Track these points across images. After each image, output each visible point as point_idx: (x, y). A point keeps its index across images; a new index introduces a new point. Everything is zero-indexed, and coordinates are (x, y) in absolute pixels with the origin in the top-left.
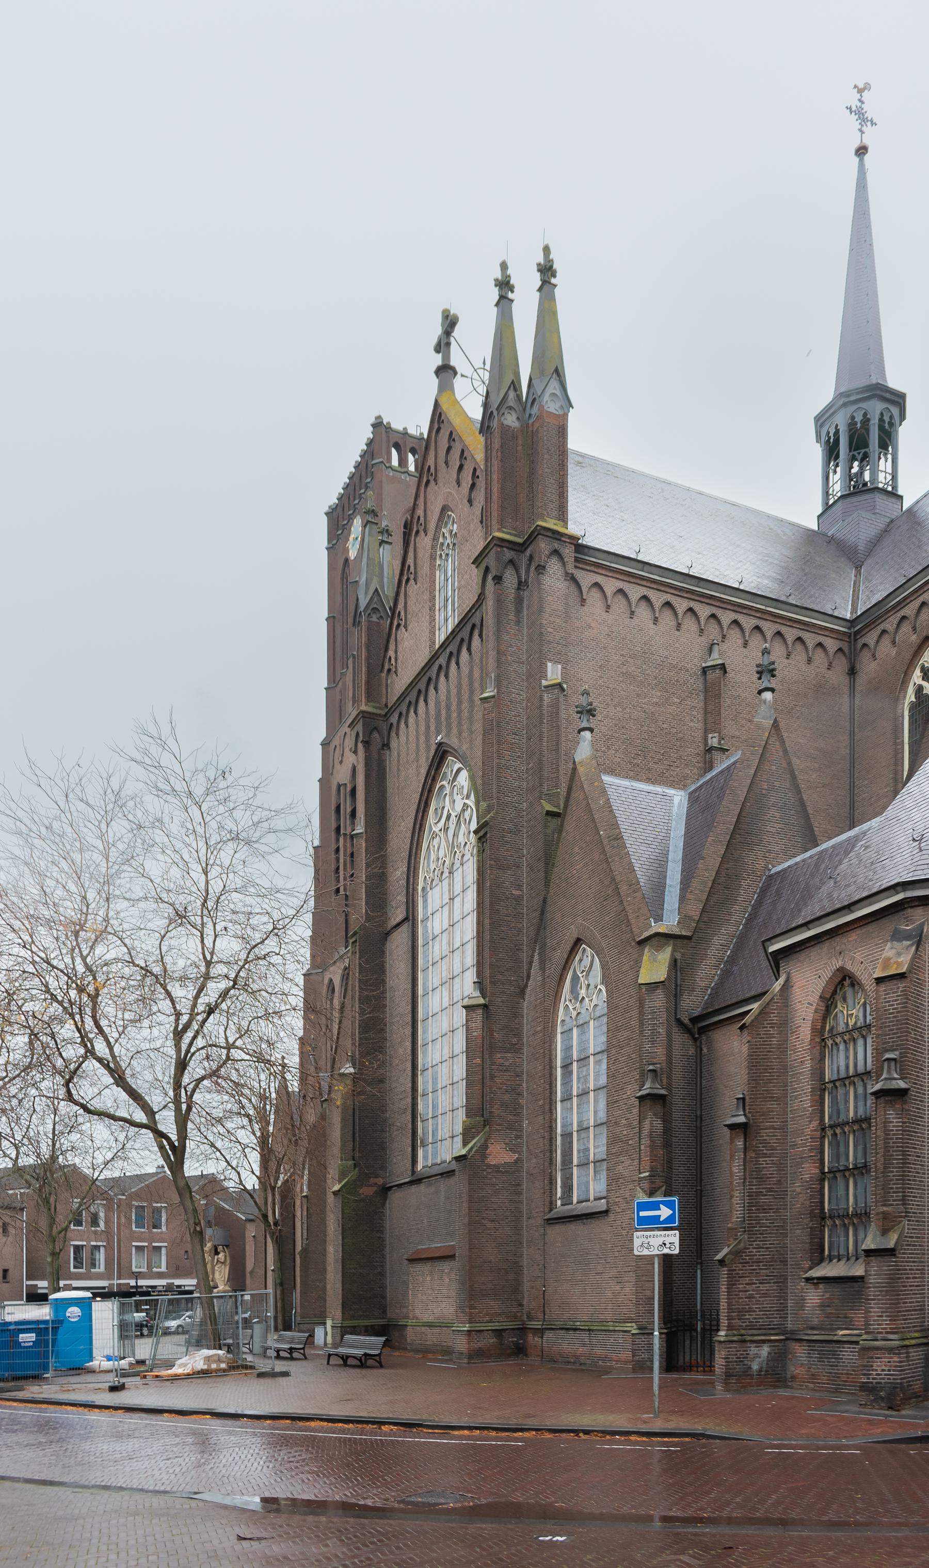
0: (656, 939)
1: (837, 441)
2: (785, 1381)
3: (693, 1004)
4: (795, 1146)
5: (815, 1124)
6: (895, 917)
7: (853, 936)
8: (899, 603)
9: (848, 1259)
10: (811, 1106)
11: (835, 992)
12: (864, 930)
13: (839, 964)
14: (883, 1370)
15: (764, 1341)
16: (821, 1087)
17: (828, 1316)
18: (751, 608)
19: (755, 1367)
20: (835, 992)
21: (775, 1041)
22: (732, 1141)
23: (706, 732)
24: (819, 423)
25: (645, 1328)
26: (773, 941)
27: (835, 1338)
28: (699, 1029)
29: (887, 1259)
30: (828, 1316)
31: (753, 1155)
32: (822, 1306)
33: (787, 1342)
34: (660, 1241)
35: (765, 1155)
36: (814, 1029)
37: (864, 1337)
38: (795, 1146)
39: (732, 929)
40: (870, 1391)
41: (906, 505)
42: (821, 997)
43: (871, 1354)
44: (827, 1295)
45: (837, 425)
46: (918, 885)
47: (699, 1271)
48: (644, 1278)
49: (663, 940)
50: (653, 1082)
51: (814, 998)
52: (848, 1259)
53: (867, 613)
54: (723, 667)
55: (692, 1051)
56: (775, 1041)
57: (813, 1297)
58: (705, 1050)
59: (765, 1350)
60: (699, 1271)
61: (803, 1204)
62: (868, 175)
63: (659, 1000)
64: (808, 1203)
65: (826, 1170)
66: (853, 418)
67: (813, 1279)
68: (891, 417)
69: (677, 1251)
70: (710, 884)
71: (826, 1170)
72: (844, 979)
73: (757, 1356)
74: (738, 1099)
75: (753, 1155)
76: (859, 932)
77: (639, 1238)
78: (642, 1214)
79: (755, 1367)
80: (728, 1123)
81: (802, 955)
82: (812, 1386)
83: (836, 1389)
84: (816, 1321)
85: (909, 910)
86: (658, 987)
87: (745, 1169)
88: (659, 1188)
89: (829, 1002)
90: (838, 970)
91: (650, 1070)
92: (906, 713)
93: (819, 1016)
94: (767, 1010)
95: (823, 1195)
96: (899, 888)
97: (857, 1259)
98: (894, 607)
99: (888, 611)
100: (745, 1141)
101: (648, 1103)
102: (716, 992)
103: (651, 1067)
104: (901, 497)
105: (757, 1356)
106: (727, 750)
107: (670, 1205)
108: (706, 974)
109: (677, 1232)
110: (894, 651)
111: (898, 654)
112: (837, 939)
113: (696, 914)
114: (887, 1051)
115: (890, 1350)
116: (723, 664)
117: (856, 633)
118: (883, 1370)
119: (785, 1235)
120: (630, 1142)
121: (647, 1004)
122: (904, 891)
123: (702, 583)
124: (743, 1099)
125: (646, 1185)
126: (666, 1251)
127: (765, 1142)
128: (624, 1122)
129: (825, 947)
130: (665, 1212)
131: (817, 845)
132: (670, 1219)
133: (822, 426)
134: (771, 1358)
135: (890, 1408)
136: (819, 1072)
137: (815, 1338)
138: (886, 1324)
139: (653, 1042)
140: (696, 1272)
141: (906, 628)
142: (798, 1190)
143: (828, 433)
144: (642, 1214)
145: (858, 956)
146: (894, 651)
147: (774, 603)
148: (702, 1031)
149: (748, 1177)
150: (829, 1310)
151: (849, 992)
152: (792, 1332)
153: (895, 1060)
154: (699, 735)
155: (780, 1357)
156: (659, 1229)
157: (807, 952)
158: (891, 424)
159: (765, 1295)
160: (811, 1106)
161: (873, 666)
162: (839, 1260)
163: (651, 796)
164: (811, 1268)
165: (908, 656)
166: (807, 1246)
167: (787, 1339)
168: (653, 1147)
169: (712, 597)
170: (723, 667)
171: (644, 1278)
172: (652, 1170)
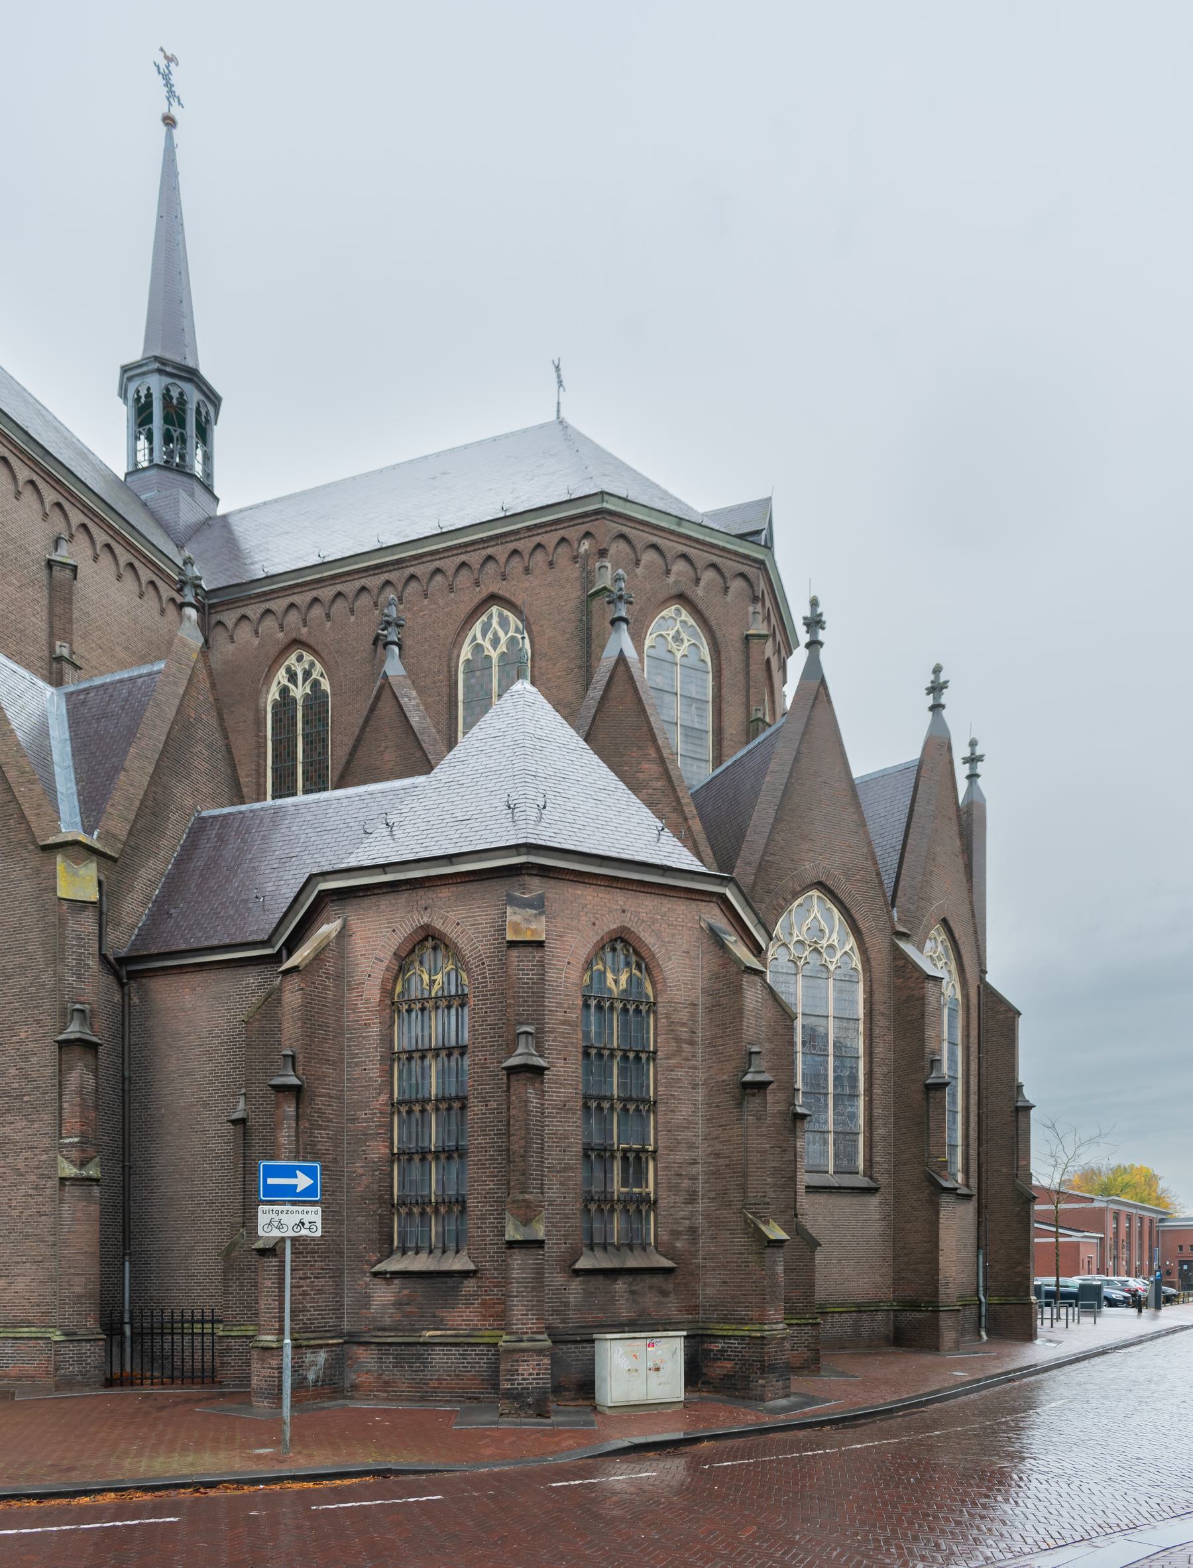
0: (76, 848)
1: (149, 404)
2: (342, 1391)
3: (121, 941)
4: (353, 1120)
5: (384, 1097)
6: (507, 881)
7: (445, 893)
8: (264, 594)
9: (431, 1252)
10: (380, 1077)
11: (413, 951)
12: (461, 888)
13: (425, 920)
14: (531, 1374)
15: (321, 1346)
16: (391, 1057)
17: (407, 1315)
18: (103, 520)
19: (311, 1376)
20: (413, 951)
21: (330, 995)
22: (278, 1105)
23: (52, 636)
24: (126, 375)
25: (75, 1334)
26: (328, 877)
27: (421, 1340)
28: (128, 973)
29: (533, 1251)
30: (407, 1315)
31: (307, 1125)
32: (398, 1304)
33: (346, 1346)
34: (296, 1219)
35: (320, 1127)
36: (384, 990)
37: (506, 1338)
38: (353, 1120)
39: (160, 866)
40: (515, 1398)
41: (221, 510)
42: (395, 954)
43: (516, 1356)
44: (406, 1292)
45: (149, 389)
46: (543, 852)
47: (127, 1264)
48: (72, 1271)
49: (84, 852)
50: (81, 1025)
51: (387, 955)
52: (431, 1252)
53: (226, 591)
54: (74, 569)
55: (117, 998)
56: (330, 995)
57: (383, 1295)
58: (135, 1000)
59: (322, 1356)
60: (127, 1264)
61: (367, 1187)
62: (177, 151)
63: (87, 923)
64: (376, 1187)
65: (396, 1151)
66: (168, 390)
67: (386, 1273)
68: (207, 413)
69: (319, 1234)
70: (137, 803)
71: (396, 1151)
72: (426, 939)
73: (313, 1364)
74: (285, 1056)
75: (307, 1125)
76: (453, 889)
77: (264, 1215)
78: (270, 1181)
79: (311, 1376)
80: (273, 1082)
81: (367, 902)
82: (385, 1395)
83: (421, 1397)
84: (388, 1321)
85: (527, 878)
86: (86, 907)
87: (297, 1141)
88: (92, 1159)
89: (404, 961)
90: (422, 927)
91: (77, 1010)
92: (269, 709)
93: (390, 975)
94: (322, 957)
95: (392, 1179)
96: (523, 850)
97: (444, 1252)
98: (258, 595)
99: (250, 597)
100: (298, 1108)
101: (77, 1051)
102: (146, 934)
103: (78, 1006)
104: (217, 500)
105: (313, 1364)
106: (80, 668)
107: (310, 1172)
108: (134, 910)
109: (319, 1209)
110: (256, 642)
111: (261, 646)
112: (421, 892)
113: (123, 834)
114: (522, 1024)
115: (540, 1352)
116: (76, 567)
117: (211, 606)
118: (531, 1374)
119: (341, 1222)
120: (26, 1099)
121: (71, 925)
122: (527, 854)
123: (48, 458)
124: (293, 1057)
125: (74, 1153)
126: (304, 1232)
127: (319, 1111)
128: (13, 1071)
129: (403, 898)
130: (302, 1181)
131: (243, 803)
132: (310, 1191)
133: (130, 379)
134: (328, 1366)
135: (539, 1415)
136: (387, 1039)
137: (389, 1340)
138: (532, 1323)
139: (79, 976)
140: (123, 1264)
141: (270, 623)
142: (360, 1171)
143: (138, 392)
144: (270, 1181)
145: (453, 916)
146: (256, 642)
147: (130, 529)
148: (132, 975)
149: (301, 1150)
150: (408, 1309)
151: (428, 955)
152: (350, 1334)
153: (531, 1034)
154: (43, 636)
155: (337, 1364)
156: (294, 1203)
157: (374, 899)
158: (207, 421)
159: (320, 1292)
160: (380, 1077)
161: (231, 648)
162: (417, 1253)
163: (16, 677)
164: (380, 1261)
165: (274, 651)
166: (375, 1236)
167: (346, 1343)
168: (83, 1106)
169: (58, 481)
170: (74, 569)
171: (72, 1271)
172: (83, 1135)
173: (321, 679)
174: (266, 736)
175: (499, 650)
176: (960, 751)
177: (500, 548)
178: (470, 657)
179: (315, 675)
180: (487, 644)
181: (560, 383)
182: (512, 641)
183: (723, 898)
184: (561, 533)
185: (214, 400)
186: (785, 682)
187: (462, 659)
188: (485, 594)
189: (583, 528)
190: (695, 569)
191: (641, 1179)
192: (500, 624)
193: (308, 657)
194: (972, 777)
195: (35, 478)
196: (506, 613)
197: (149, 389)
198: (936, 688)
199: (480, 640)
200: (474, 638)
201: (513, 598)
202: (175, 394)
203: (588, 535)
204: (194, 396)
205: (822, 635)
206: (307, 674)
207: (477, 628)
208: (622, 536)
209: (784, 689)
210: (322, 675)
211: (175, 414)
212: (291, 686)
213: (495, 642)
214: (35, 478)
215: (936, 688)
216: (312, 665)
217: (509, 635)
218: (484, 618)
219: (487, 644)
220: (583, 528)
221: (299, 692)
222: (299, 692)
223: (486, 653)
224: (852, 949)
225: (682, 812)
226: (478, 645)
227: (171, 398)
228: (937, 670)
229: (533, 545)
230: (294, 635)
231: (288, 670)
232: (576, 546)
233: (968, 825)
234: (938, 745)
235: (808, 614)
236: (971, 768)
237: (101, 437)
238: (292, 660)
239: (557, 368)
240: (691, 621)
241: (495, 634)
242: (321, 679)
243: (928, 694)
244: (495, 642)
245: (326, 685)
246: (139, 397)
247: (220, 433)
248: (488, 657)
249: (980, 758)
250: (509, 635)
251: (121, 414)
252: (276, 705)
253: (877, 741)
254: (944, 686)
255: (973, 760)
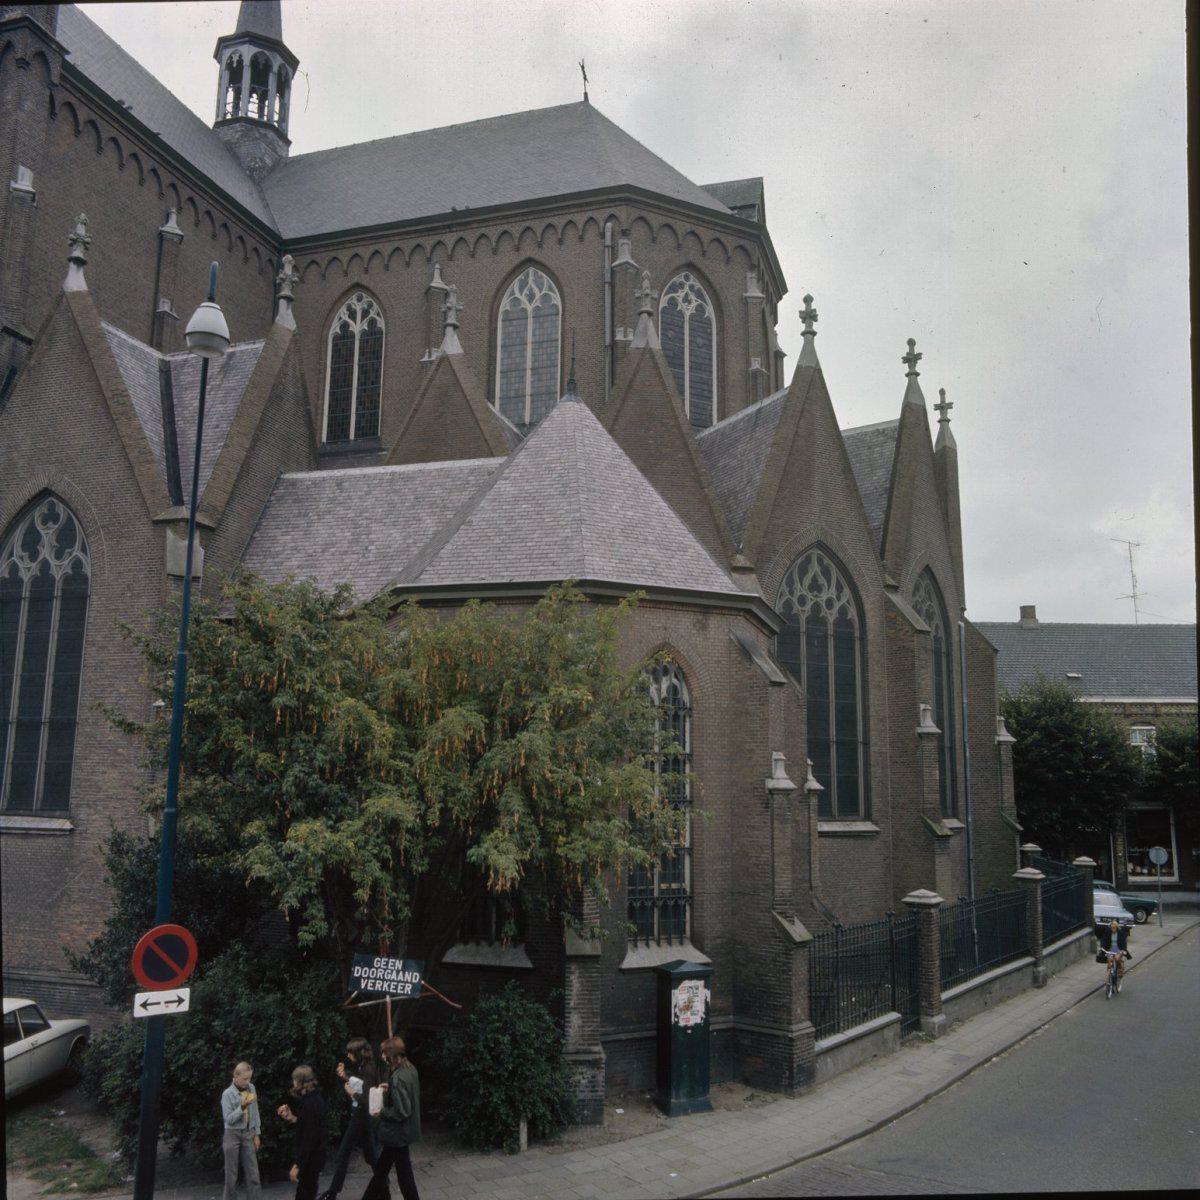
45: (240, 56)
173: (377, 318)
174: (326, 364)
175: (534, 305)
176: (931, 400)
177: (537, 221)
178: (508, 308)
179: (372, 314)
180: (523, 298)
181: (585, 78)
182: (546, 298)
183: (749, 612)
184: (590, 214)
185: (292, 62)
186: (776, 322)
187: (501, 309)
188: (522, 258)
189: (609, 211)
190: (702, 243)
191: (678, 877)
192: (535, 282)
193: (367, 298)
194: (944, 421)
195: (157, 166)
196: (540, 273)
197: (240, 56)
198: (911, 359)
199: (517, 295)
200: (513, 293)
201: (547, 263)
202: (262, 61)
203: (612, 217)
204: (277, 62)
205: (816, 326)
206: (365, 313)
207: (516, 284)
208: (641, 218)
209: (776, 329)
210: (378, 314)
211: (260, 71)
212: (351, 322)
213: (531, 297)
214: (157, 166)
215: (911, 359)
216: (370, 305)
217: (543, 292)
218: (522, 276)
219: (523, 298)
220: (609, 211)
221: (357, 327)
222: (357, 327)
223: (523, 306)
224: (848, 602)
225: (699, 481)
226: (517, 299)
227: (258, 64)
228: (911, 343)
229: (565, 221)
230: (356, 280)
231: (349, 308)
232: (602, 225)
233: (942, 466)
234: (913, 409)
235: (804, 309)
236: (942, 413)
237: (199, 89)
238: (353, 300)
239: (583, 67)
240: (698, 285)
241: (531, 290)
242: (377, 318)
243: (904, 362)
244: (531, 297)
245: (381, 324)
246: (232, 62)
247: (297, 83)
248: (524, 310)
249: (950, 406)
250: (543, 292)
251: (213, 70)
252: (336, 338)
253: (861, 403)
254: (919, 356)
255: (943, 407)
